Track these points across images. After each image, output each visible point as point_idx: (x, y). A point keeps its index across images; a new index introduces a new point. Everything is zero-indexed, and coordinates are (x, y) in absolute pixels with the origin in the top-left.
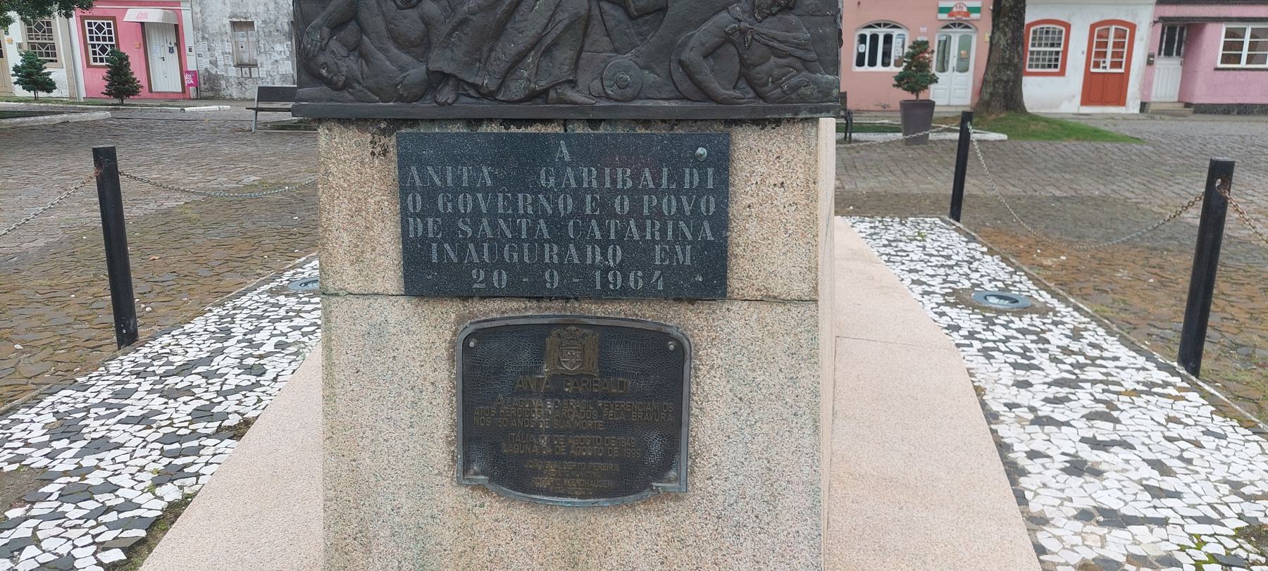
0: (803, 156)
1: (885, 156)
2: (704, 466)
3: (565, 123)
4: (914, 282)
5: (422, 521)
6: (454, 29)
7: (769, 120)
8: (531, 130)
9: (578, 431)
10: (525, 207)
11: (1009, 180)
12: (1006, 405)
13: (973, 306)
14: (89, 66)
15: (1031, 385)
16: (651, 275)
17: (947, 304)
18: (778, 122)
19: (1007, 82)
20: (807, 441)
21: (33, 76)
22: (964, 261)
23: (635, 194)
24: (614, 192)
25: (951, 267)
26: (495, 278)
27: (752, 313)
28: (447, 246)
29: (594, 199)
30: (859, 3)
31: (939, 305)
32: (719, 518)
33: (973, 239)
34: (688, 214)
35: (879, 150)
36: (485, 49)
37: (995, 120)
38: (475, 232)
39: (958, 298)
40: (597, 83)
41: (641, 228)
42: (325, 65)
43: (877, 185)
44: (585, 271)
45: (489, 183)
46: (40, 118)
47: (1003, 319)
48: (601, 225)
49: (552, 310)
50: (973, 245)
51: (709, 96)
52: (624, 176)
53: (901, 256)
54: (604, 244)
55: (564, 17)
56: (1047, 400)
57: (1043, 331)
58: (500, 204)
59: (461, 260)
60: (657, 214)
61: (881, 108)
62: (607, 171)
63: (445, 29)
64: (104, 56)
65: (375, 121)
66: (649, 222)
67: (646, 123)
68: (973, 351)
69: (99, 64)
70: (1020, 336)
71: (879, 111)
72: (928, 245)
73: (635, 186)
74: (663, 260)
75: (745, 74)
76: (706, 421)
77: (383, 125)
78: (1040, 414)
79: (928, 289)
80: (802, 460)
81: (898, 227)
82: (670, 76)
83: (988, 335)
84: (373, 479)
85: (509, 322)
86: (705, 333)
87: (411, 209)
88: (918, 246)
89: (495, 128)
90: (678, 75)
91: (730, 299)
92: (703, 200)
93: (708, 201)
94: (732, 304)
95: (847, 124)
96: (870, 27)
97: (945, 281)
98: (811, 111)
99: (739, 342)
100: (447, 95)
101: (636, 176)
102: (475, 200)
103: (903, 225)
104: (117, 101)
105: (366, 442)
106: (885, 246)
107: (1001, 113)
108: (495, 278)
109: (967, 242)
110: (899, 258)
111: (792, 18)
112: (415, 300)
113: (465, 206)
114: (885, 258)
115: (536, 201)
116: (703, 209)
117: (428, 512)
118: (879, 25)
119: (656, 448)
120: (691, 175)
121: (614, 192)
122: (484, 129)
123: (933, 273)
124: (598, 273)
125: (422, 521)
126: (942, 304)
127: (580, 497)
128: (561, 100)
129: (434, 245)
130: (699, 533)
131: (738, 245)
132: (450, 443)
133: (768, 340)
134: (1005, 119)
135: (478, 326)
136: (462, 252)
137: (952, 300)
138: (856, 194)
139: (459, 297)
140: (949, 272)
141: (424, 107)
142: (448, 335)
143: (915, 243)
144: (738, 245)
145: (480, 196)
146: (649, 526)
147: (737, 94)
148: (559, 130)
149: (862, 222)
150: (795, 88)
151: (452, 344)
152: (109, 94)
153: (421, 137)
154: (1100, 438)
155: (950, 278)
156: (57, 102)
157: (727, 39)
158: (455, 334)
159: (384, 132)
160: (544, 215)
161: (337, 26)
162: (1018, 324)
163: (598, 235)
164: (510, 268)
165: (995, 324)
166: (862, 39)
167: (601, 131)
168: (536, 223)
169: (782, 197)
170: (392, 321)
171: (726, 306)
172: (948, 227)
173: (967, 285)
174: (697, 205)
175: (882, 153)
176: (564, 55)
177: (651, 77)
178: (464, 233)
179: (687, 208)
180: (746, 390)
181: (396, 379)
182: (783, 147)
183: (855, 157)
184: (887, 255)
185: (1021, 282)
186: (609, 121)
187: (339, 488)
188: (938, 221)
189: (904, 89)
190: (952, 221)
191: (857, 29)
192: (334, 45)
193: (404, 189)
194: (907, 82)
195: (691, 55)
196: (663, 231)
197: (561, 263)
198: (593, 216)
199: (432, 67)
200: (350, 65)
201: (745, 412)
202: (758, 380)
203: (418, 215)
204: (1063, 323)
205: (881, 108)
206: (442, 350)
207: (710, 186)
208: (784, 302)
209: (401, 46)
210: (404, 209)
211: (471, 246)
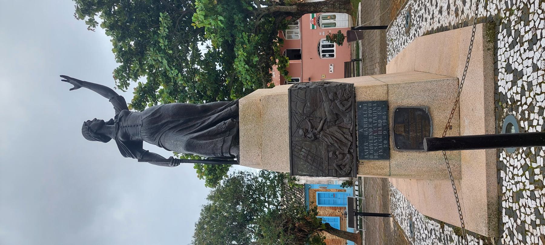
0: (361, 89)
1: (367, 46)
2: (423, 103)
3: (356, 130)
4: (404, 45)
5: (438, 159)
6: (341, 149)
7: (355, 95)
8: (358, 136)
9: (416, 127)
10: (371, 137)
11: (375, 5)
12: (430, 26)
13: (410, 29)
15: (426, 18)
17: (409, 36)
18: (355, 94)
19: (340, 4)
20: (416, 84)
22: (398, 28)
23: (368, 118)
24: (368, 121)
25: (400, 32)
26: (385, 143)
27: (390, 96)
29: (369, 125)
30: (311, 59)
31: (409, 38)
33: (392, 23)
34: (372, 108)
35: (366, 48)
36: (344, 144)
37: (354, 7)
38: (376, 146)
39: (408, 32)
40: (349, 125)
41: (374, 117)
42: (348, 171)
43: (377, 51)
44: (383, 127)
45: (367, 144)
47: (412, 21)
50: (394, 24)
51: (351, 106)
52: (365, 120)
53: (397, 47)
55: (338, 130)
56: (429, 14)
57: (415, 10)
61: (350, 46)
62: (364, 123)
63: (341, 150)
65: (357, 164)
66: (373, 115)
67: (356, 116)
68: (419, 31)
70: (416, 17)
71: (351, 46)
72: (394, 38)
73: (367, 118)
75: (347, 100)
77: (358, 163)
78: (431, 17)
79: (406, 41)
81: (389, 47)
82: (347, 112)
83: (416, 26)
84: (429, 168)
85: (394, 141)
87: (372, 158)
88: (395, 42)
89: (358, 143)
90: (347, 111)
95: (356, 61)
96: (319, 54)
97: (404, 35)
98: (353, 88)
100: (352, 151)
101: (365, 118)
102: (370, 146)
103: (389, 45)
105: (421, 169)
106: (395, 52)
107: (351, 5)
108: (385, 143)
109: (393, 26)
110: (398, 48)
111: (338, 93)
112: (391, 158)
113: (372, 148)
114: (398, 52)
115: (370, 135)
116: (371, 106)
117: (436, 157)
118: (319, 50)
119: (419, 113)
120: (364, 108)
121: (368, 121)
122: (358, 145)
123: (401, 38)
124: (384, 124)
126: (409, 37)
127: (430, 127)
128: (352, 131)
129: (379, 154)
131: (377, 99)
132: (420, 153)
134: (353, 3)
135: (395, 146)
136: (380, 149)
137: (408, 34)
138: (381, 58)
139: (389, 150)
140: (401, 33)
141: (354, 154)
142: (397, 152)
143: (394, 42)
144: (377, 99)
145: (370, 145)
147: (350, 101)
148: (357, 131)
149: (388, 58)
150: (349, 91)
151: (399, 151)
153: (359, 155)
154: (435, 4)
155: (403, 33)
157: (341, 103)
158: (397, 151)
159: (359, 162)
161: (341, 169)
162: (413, 17)
164: (383, 140)
165: (413, 23)
166: (324, 56)
167: (357, 124)
168: (374, 135)
169: (368, 92)
170: (395, 163)
172: (389, 30)
173: (404, 29)
174: (370, 107)
175: (367, 47)
176: (344, 130)
178: (377, 148)
179: (371, 108)
180: (406, 96)
183: (368, 57)
184: (397, 52)
185: (403, 12)
186: (356, 123)
187: (431, 175)
188: (388, 33)
189: (343, 42)
190: (387, 29)
191: (320, 58)
192: (344, 170)
193: (369, 159)
194: (341, 41)
195: (344, 110)
196: (375, 113)
197: (382, 131)
199: (347, 153)
200: (347, 167)
201: (411, 96)
202: (404, 94)
203: (374, 156)
204: (413, 4)
205: (350, 46)
206: (400, 154)
208: (388, 90)
209: (344, 158)
210: (373, 159)
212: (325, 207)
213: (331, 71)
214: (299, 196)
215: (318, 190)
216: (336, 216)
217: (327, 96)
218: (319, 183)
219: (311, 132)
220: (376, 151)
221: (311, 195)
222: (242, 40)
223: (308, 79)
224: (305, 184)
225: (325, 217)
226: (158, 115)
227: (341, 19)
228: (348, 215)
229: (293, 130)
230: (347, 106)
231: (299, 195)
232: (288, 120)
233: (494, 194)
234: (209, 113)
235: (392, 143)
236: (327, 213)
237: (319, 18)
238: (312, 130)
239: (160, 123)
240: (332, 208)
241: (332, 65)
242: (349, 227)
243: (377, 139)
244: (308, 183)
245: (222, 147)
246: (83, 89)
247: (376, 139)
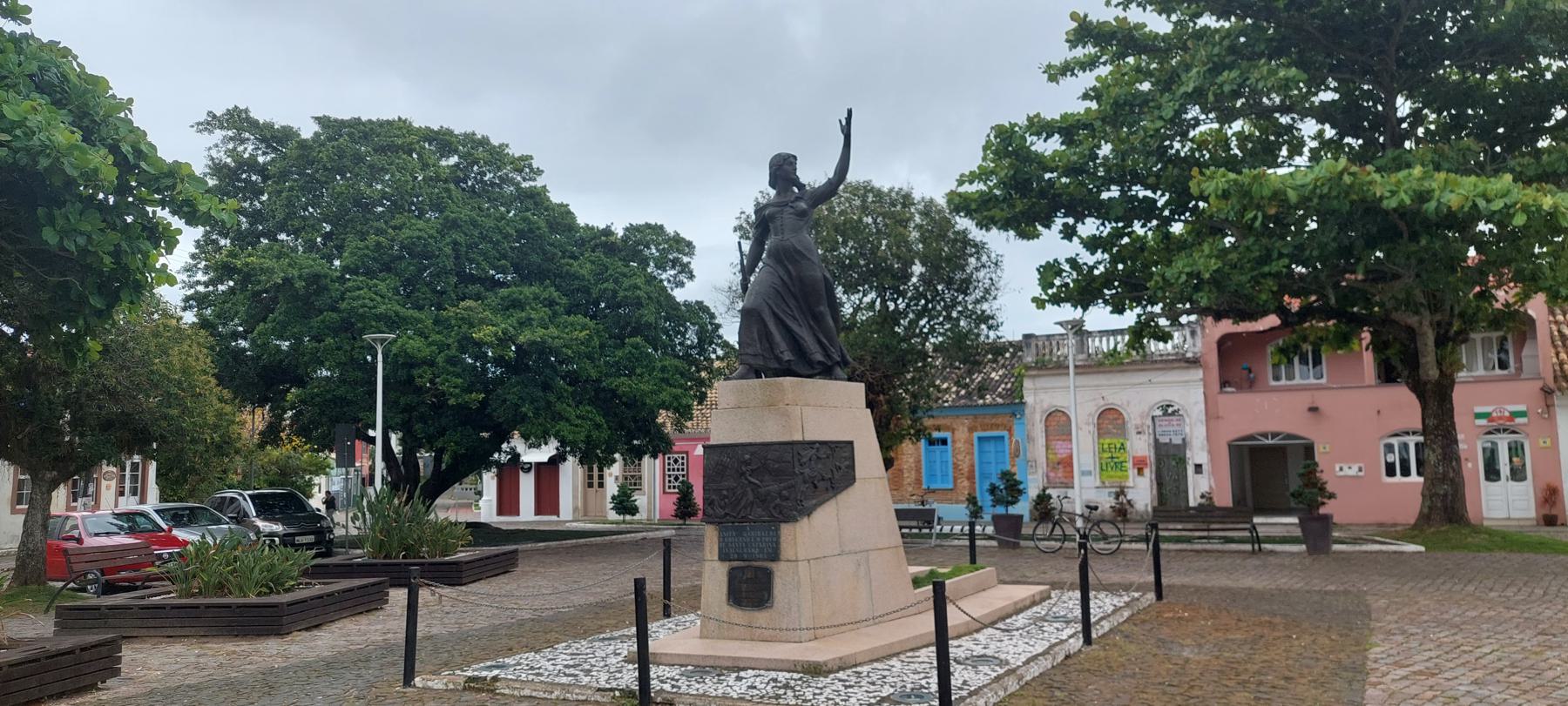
14: (664, 492)
19: (1445, 495)
21: (624, 504)
23: (761, 537)
30: (1379, 412)
37: (1433, 533)
46: (628, 535)
49: (747, 563)
64: (676, 484)
69: (672, 490)
96: (1396, 435)
104: (681, 522)
118: (1407, 433)
119: (766, 596)
134: (1447, 531)
152: (676, 516)
156: (638, 523)
161: (710, 504)
166: (1389, 448)
191: (1382, 438)
200: (711, 512)
212: (973, 454)
213: (1341, 469)
214: (1000, 390)
215: (1011, 435)
216: (955, 479)
217: (785, 489)
218: (1030, 439)
220: (727, 545)
221: (999, 421)
222: (1275, 255)
223: (1315, 405)
224: (1024, 403)
225: (950, 454)
226: (798, 258)
227: (1510, 498)
228: (921, 507)
229: (749, 448)
230: (773, 512)
231: (1003, 389)
232: (762, 441)
233: (664, 660)
234: (812, 323)
235: (736, 564)
236: (960, 457)
237: (1514, 432)
239: (786, 263)
240: (972, 471)
241: (1360, 470)
242: (518, 515)
244: (1027, 411)
245: (747, 354)
246: (842, 137)
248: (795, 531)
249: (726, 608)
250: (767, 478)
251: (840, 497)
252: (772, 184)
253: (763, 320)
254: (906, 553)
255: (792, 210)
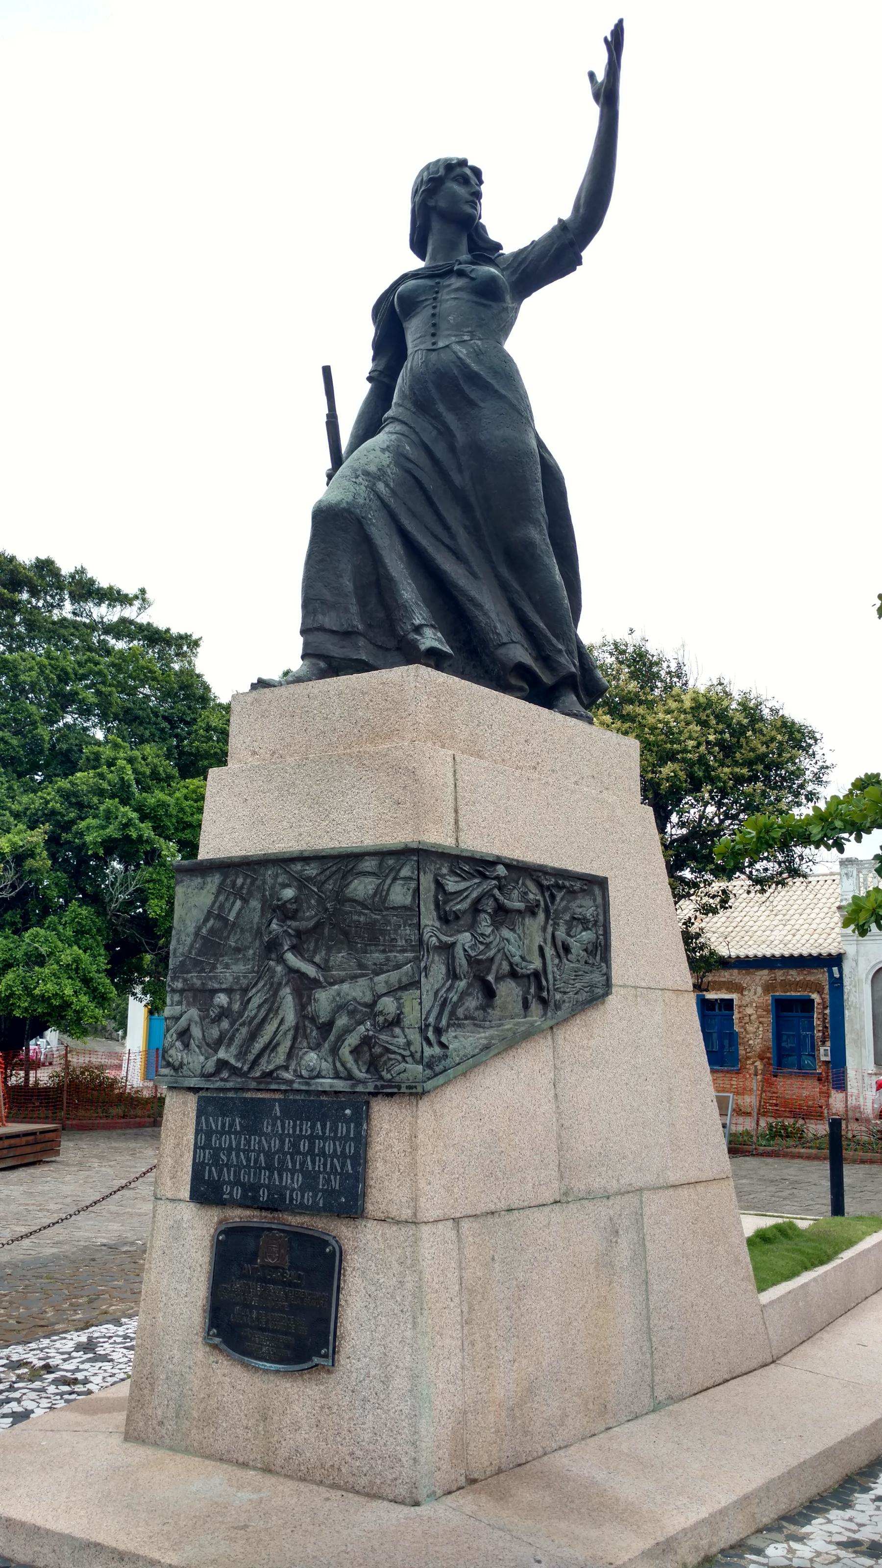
16: (317, 1196)
23: (312, 1139)
24: (301, 1137)
28: (213, 1169)
29: (290, 1141)
32: (353, 1392)
38: (228, 1160)
45: (238, 1129)
48: (292, 1158)
54: (293, 1172)
58: (242, 1142)
59: (219, 1178)
60: (322, 1153)
66: (317, 1158)
74: (323, 1185)
76: (349, 1311)
80: (406, 1349)
84: (162, 1334)
86: (351, 1243)
91: (367, 1218)
92: (348, 1145)
93: (350, 1146)
94: (367, 1222)
99: (370, 1251)
100: (225, 1074)
101: (313, 1127)
102: (230, 1139)
108: (235, 1192)
115: (260, 1141)
117: (188, 1363)
120: (342, 1127)
124: (288, 1192)
125: (184, 1370)
130: (340, 1403)
133: (388, 1251)
136: (220, 1173)
145: (233, 1136)
146: (310, 1393)
160: (263, 1151)
163: (290, 1167)
164: (243, 1185)
168: (259, 1156)
170: (185, 1219)
171: (364, 1223)
177: (324, 1065)
178: (223, 1161)
179: (339, 1150)
181: (183, 1260)
182: (398, 1111)
196: (325, 1165)
198: (289, 1153)
201: (372, 1306)
207: (352, 1136)
211: (225, 1169)
219: (285, 928)
220: (215, 1157)
226: (474, 394)
234: (504, 571)
235: (237, 1215)
238: (289, 935)
239: (441, 408)
243: (248, 1166)
246: (594, 111)
247: (248, 1160)
248: (414, 1125)
249: (200, 1353)
250: (305, 946)
251: (561, 1034)
252: (418, 245)
253: (367, 540)
254: (224, 734)
255: (456, 282)
